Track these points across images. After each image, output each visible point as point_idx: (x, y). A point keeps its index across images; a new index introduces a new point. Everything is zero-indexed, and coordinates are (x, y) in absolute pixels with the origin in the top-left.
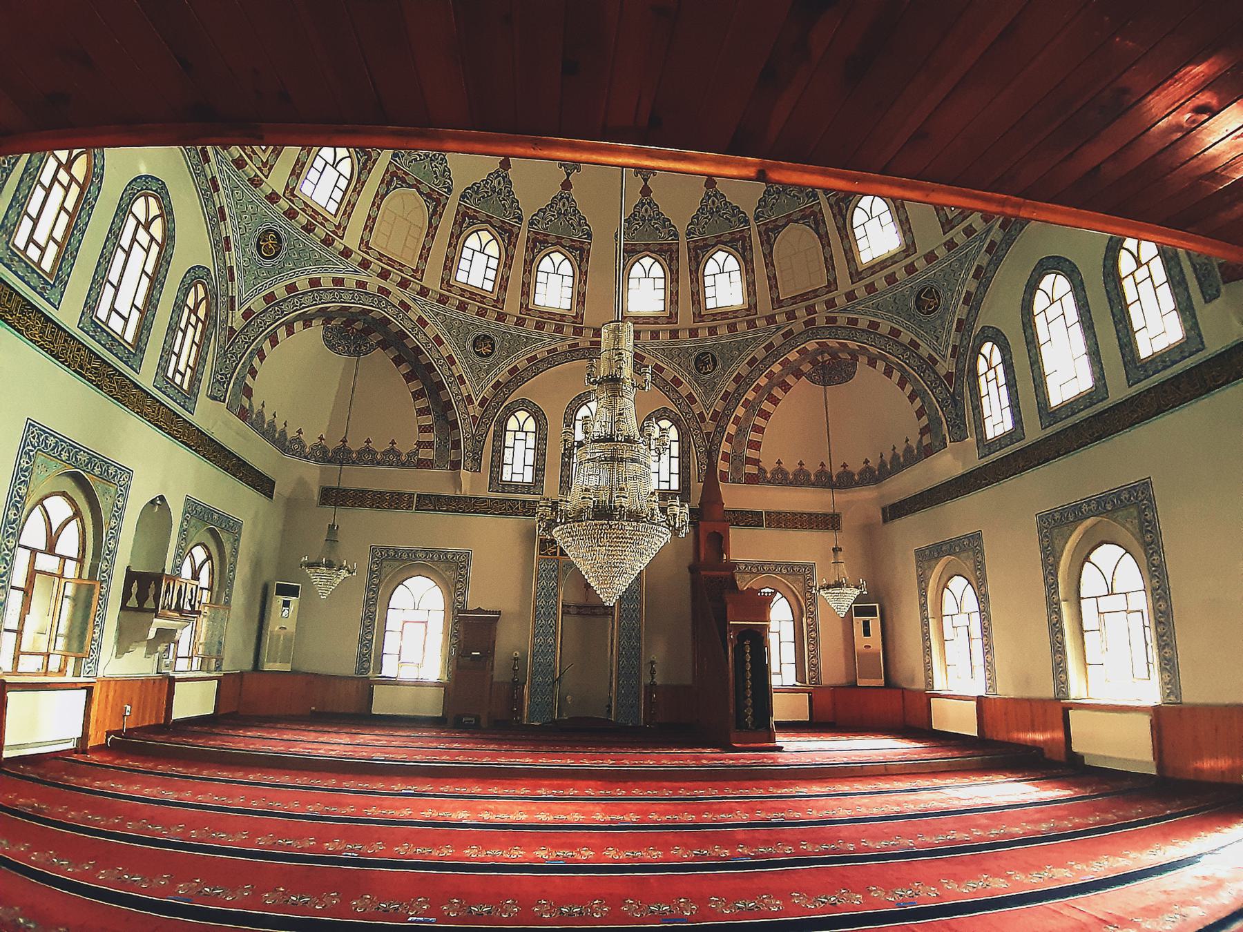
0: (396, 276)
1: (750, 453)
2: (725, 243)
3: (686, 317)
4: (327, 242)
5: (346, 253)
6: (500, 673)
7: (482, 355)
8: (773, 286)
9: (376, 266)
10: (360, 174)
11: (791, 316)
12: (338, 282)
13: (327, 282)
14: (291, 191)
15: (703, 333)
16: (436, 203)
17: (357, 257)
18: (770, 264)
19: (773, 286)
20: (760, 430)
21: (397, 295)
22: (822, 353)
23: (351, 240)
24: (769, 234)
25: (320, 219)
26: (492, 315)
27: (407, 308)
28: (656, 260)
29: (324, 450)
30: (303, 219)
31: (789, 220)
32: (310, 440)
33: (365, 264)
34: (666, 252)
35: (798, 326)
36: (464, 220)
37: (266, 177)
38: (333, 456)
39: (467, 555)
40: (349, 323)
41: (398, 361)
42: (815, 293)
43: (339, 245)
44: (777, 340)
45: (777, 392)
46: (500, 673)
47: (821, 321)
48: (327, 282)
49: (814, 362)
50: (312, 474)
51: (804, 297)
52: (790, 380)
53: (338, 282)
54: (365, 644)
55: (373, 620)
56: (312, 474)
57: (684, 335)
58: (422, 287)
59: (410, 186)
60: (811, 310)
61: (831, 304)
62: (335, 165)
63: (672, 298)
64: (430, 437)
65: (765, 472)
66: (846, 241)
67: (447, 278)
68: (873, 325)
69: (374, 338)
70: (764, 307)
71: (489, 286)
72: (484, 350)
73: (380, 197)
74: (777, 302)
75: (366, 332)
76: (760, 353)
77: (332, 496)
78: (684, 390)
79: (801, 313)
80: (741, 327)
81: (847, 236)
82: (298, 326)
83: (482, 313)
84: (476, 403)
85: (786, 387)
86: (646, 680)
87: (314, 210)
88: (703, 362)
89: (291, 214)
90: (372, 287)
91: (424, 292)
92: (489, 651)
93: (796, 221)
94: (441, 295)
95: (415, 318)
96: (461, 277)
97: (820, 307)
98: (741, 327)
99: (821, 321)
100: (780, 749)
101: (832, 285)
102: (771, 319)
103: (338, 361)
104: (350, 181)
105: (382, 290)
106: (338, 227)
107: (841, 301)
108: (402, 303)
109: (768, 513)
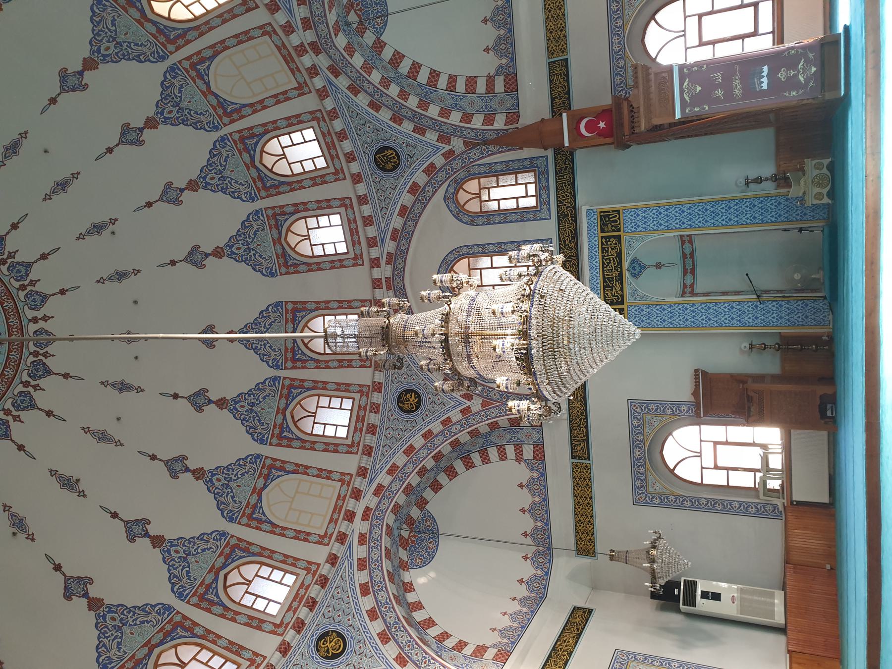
0: (351, 504)
1: (481, 87)
2: (253, 158)
3: (343, 189)
4: (323, 582)
5: (333, 560)
6: (770, 364)
7: (419, 402)
8: (281, 98)
9: (343, 526)
10: (254, 554)
11: (313, 71)
12: (362, 564)
13: (362, 577)
14: (278, 628)
15: (355, 167)
16: (274, 470)
17: (336, 548)
18: (260, 106)
19: (281, 98)
20: (453, 79)
21: (369, 500)
22: (348, 24)
23: (319, 554)
24: (229, 111)
25: (302, 592)
26: (377, 398)
27: (380, 487)
28: (288, 230)
29: (537, 554)
30: (303, 612)
31: (208, 91)
32: (528, 570)
33: (342, 538)
34: (277, 221)
35: (323, 61)
36: (285, 437)
37: (265, 658)
38: (543, 550)
39: (635, 503)
40: (404, 543)
41: (436, 487)
42: (281, 48)
43: (325, 569)
44: (343, 82)
45: (405, 67)
46: (770, 364)
47: (309, 37)
48: (362, 577)
49: (361, 31)
50: (565, 564)
51: (288, 59)
52: (387, 54)
53: (362, 564)
54: (743, 510)
55: (716, 502)
56: (565, 564)
57: (361, 189)
58: (358, 475)
59: (260, 498)
60: (301, 50)
61: (288, 29)
62: (248, 583)
63: (324, 207)
64: (510, 450)
65: (501, 66)
66: (212, 24)
67: (345, 449)
68: (403, 211)
69: (415, 513)
70: (309, 103)
71: (347, 404)
72: (413, 399)
73: (277, 530)
74: (301, 89)
75: (410, 522)
76: (362, 100)
77: (585, 545)
78: (420, 178)
79: (307, 60)
80: (338, 125)
81: (207, 22)
82: (411, 597)
83: (375, 408)
84: (469, 403)
85: (398, 58)
86: (769, 188)
87: (334, 512)
88: (387, 160)
89: (299, 626)
90: (364, 527)
91: (362, 472)
92: (739, 379)
93: (208, 84)
94: (363, 453)
95: (389, 478)
96: (342, 433)
97: (295, 40)
98: (338, 125)
99: (309, 37)
100: (847, 29)
101: (266, 30)
102: (322, 94)
103: (446, 548)
104: (262, 564)
105: (365, 517)
106: (308, 570)
107: (281, 18)
108: (377, 493)
109: (550, 53)
